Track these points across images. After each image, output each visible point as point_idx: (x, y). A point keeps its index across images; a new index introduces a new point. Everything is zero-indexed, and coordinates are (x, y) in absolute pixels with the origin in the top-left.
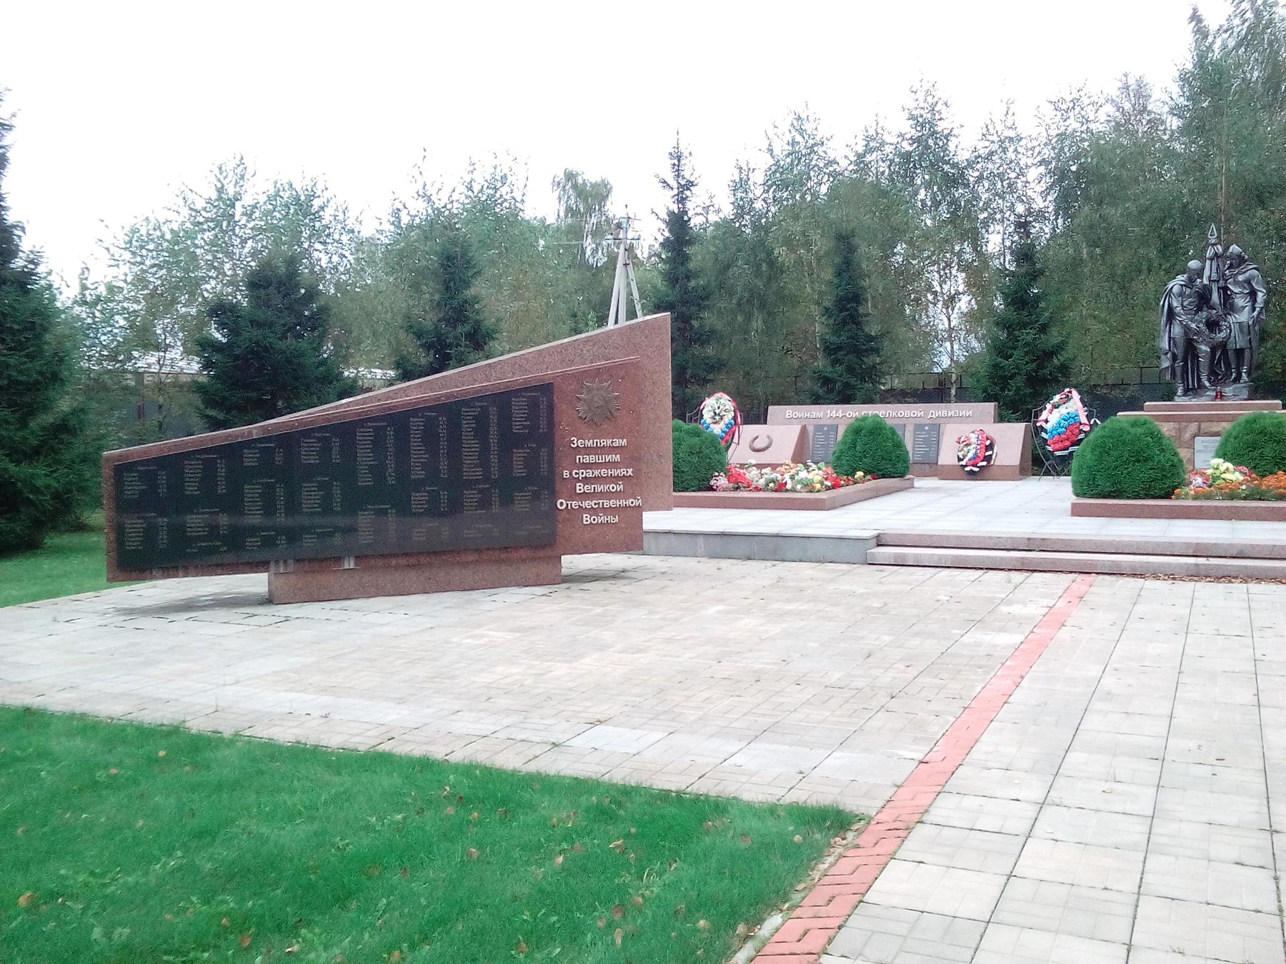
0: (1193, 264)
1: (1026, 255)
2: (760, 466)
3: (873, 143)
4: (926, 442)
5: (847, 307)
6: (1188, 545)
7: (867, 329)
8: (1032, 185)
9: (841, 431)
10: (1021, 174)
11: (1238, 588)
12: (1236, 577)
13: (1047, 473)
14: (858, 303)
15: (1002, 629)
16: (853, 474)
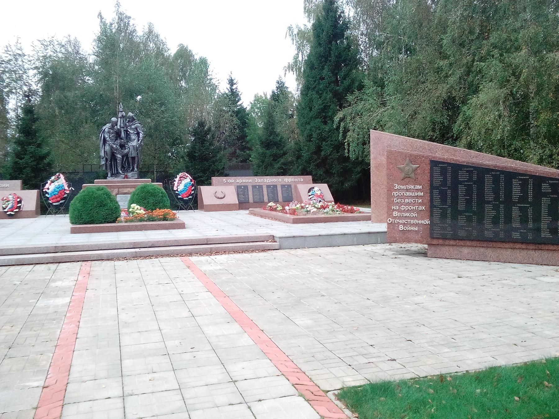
1: (30, 110)
6: (131, 243)
10: (25, 72)
12: (153, 256)
15: (57, 296)
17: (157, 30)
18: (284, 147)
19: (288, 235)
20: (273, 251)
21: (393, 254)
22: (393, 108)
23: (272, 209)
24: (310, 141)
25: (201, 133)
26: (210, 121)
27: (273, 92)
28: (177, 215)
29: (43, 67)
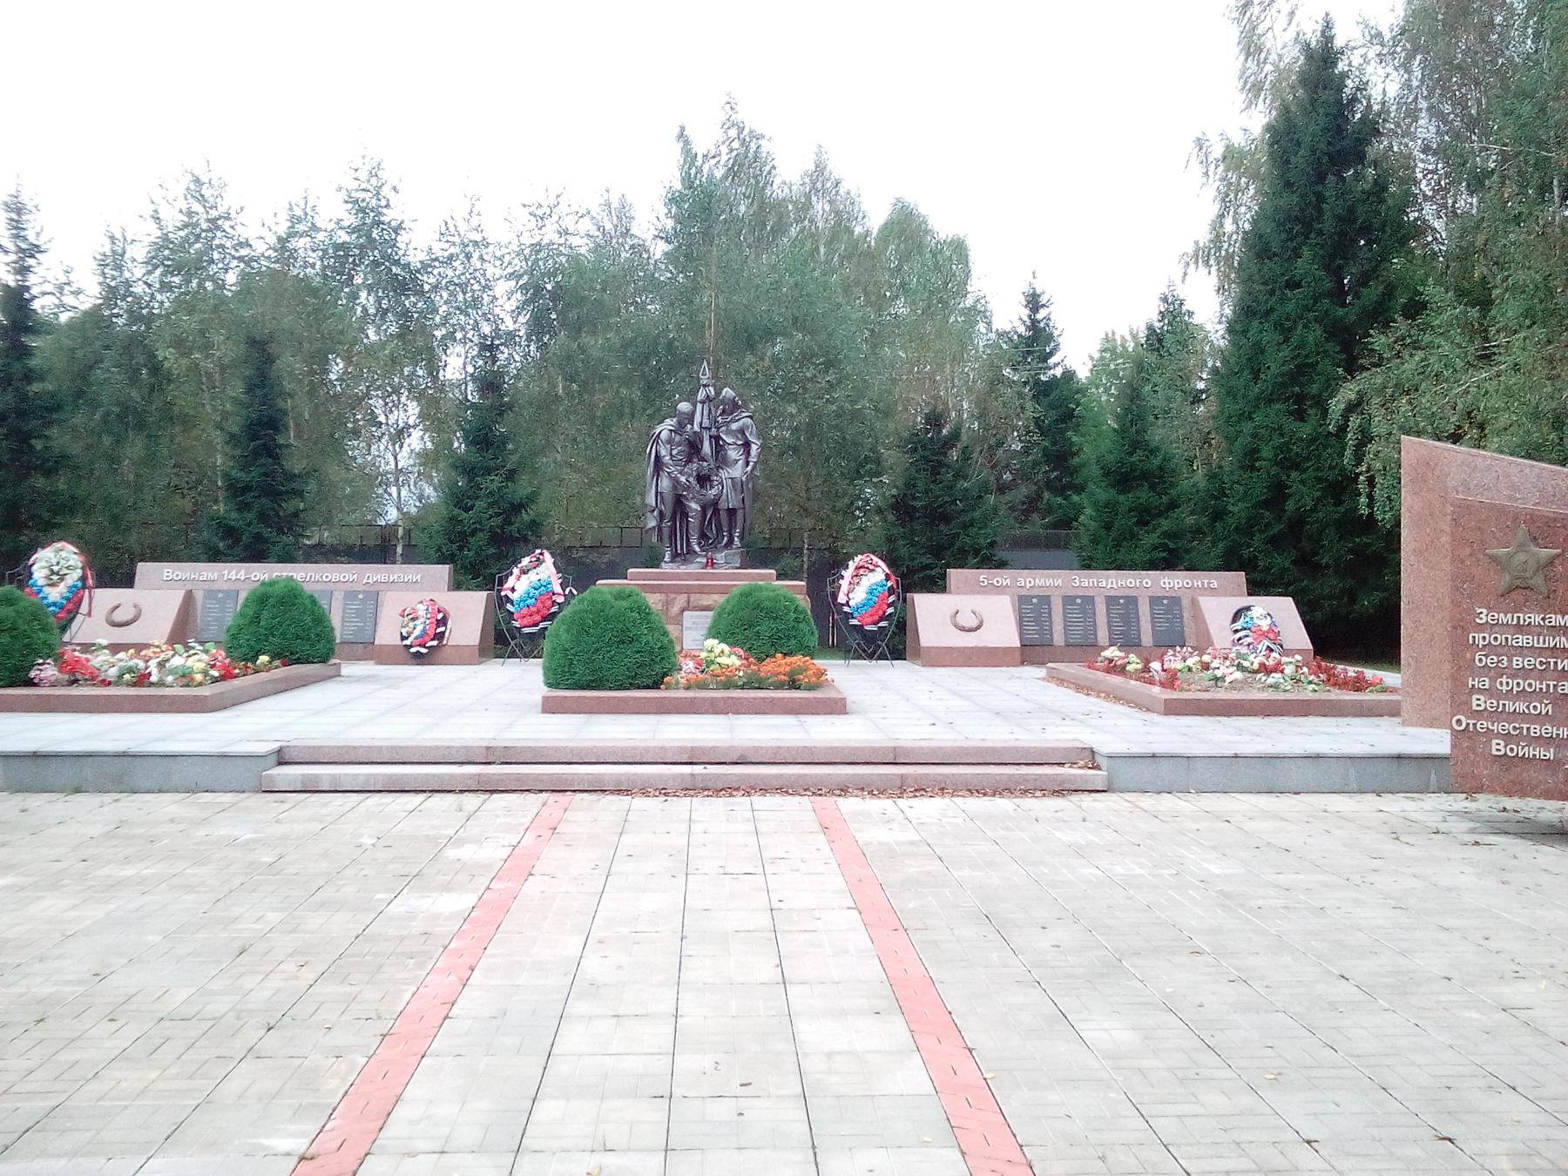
0: (684, 406)
2: (115, 648)
3: (300, 223)
4: (359, 614)
5: (262, 432)
6: (682, 750)
7: (287, 465)
8: (500, 302)
9: (241, 600)
10: (486, 288)
11: (741, 802)
12: (737, 789)
13: (513, 655)
14: (276, 430)
15: (447, 888)
16: (255, 658)
17: (837, 168)
18: (1172, 485)
19: (1136, 750)
20: (1086, 797)
21: (1472, 831)
22: (1516, 368)
23: (1114, 668)
24: (1252, 468)
25: (933, 448)
26: (963, 411)
27: (1150, 328)
28: (830, 676)
29: (531, 273)
